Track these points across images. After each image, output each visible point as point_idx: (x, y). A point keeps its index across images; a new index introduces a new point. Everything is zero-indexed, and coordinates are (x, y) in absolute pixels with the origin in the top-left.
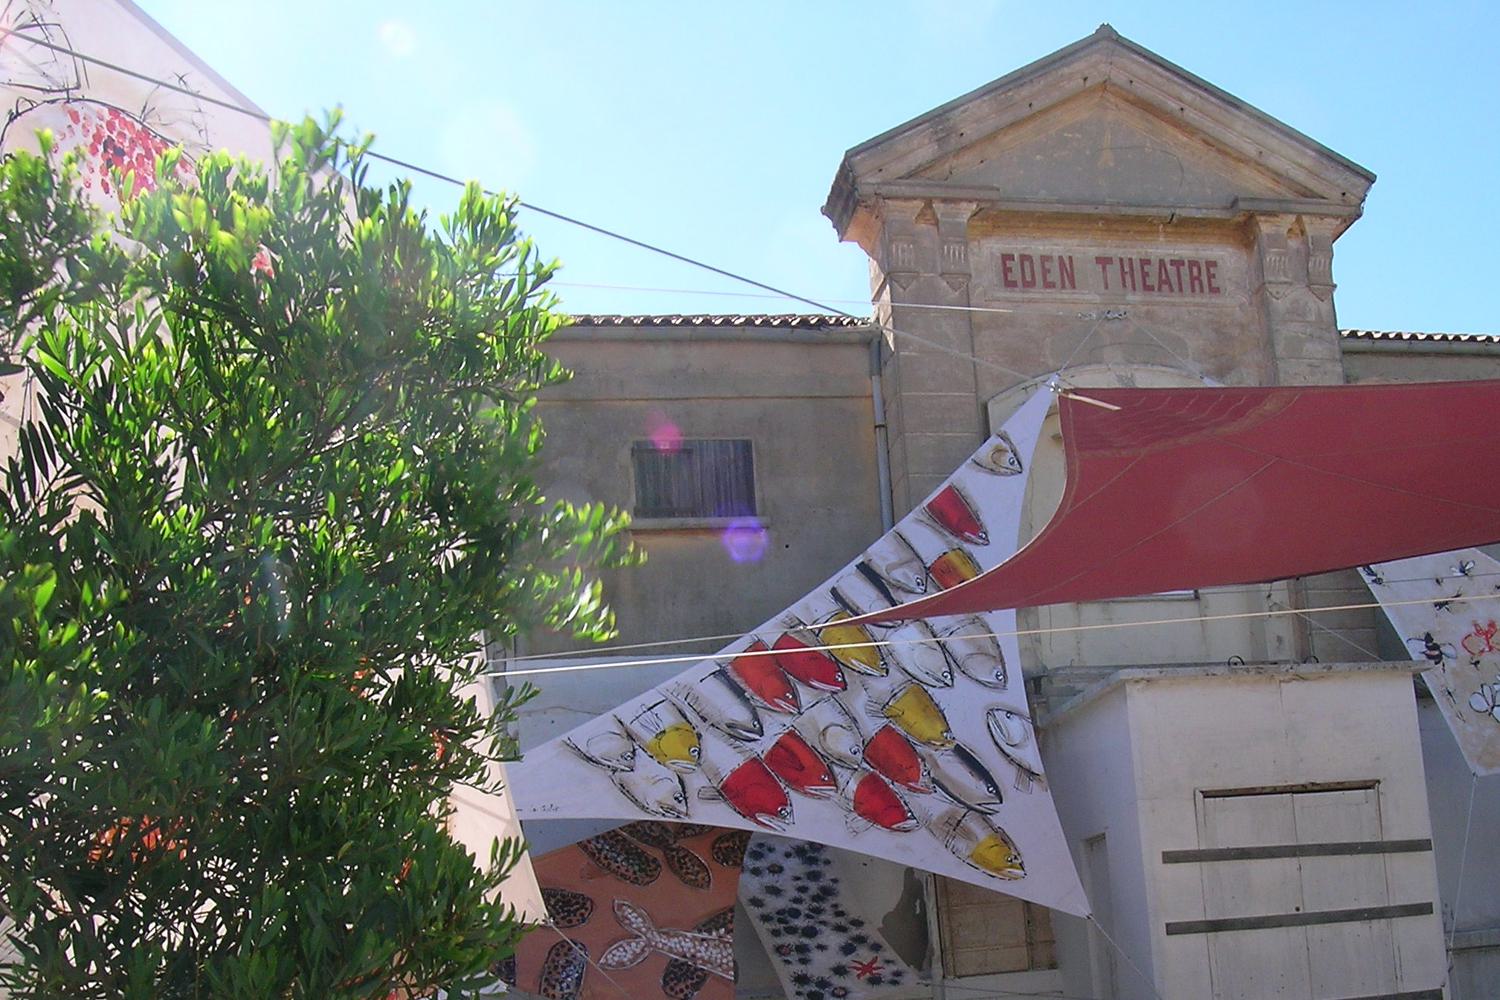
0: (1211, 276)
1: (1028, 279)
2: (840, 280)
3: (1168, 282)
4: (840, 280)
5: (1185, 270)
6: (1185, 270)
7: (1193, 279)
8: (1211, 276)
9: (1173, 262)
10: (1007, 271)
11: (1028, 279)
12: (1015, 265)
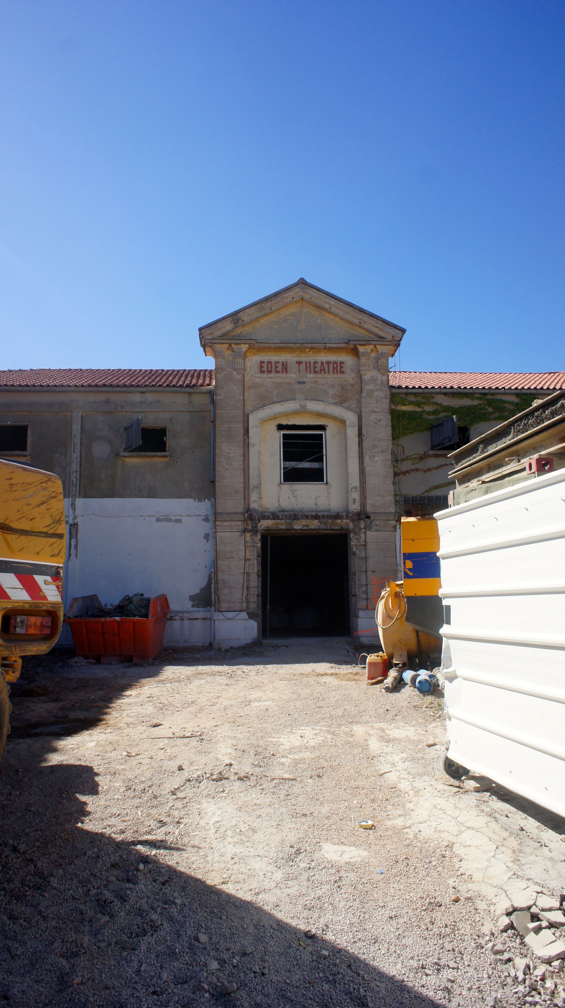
0: (341, 367)
1: (270, 370)
2: (208, 363)
3: (324, 370)
4: (208, 363)
5: (331, 365)
6: (331, 365)
7: (334, 368)
8: (341, 367)
9: (327, 363)
10: (261, 367)
11: (270, 370)
12: (265, 365)
